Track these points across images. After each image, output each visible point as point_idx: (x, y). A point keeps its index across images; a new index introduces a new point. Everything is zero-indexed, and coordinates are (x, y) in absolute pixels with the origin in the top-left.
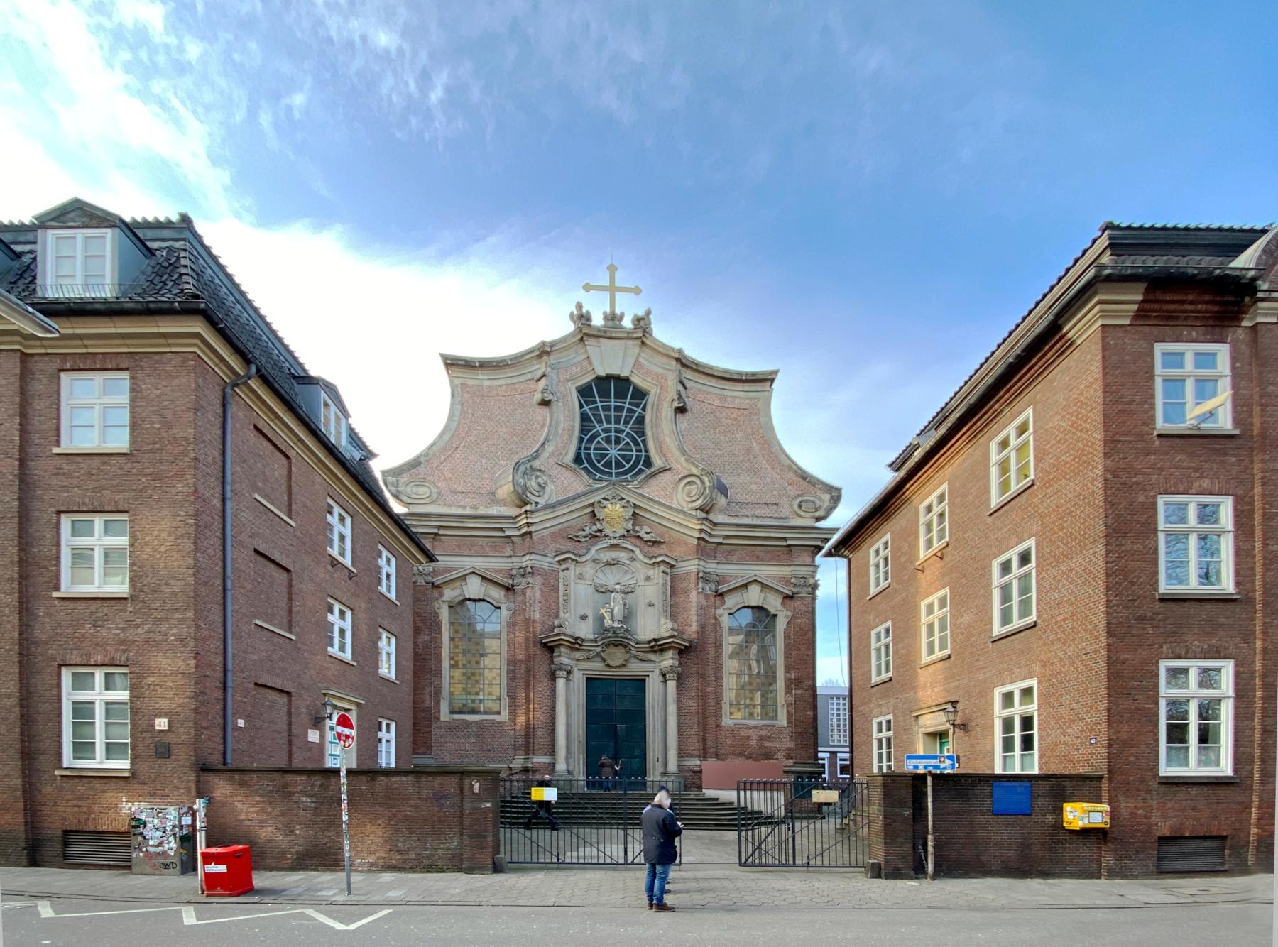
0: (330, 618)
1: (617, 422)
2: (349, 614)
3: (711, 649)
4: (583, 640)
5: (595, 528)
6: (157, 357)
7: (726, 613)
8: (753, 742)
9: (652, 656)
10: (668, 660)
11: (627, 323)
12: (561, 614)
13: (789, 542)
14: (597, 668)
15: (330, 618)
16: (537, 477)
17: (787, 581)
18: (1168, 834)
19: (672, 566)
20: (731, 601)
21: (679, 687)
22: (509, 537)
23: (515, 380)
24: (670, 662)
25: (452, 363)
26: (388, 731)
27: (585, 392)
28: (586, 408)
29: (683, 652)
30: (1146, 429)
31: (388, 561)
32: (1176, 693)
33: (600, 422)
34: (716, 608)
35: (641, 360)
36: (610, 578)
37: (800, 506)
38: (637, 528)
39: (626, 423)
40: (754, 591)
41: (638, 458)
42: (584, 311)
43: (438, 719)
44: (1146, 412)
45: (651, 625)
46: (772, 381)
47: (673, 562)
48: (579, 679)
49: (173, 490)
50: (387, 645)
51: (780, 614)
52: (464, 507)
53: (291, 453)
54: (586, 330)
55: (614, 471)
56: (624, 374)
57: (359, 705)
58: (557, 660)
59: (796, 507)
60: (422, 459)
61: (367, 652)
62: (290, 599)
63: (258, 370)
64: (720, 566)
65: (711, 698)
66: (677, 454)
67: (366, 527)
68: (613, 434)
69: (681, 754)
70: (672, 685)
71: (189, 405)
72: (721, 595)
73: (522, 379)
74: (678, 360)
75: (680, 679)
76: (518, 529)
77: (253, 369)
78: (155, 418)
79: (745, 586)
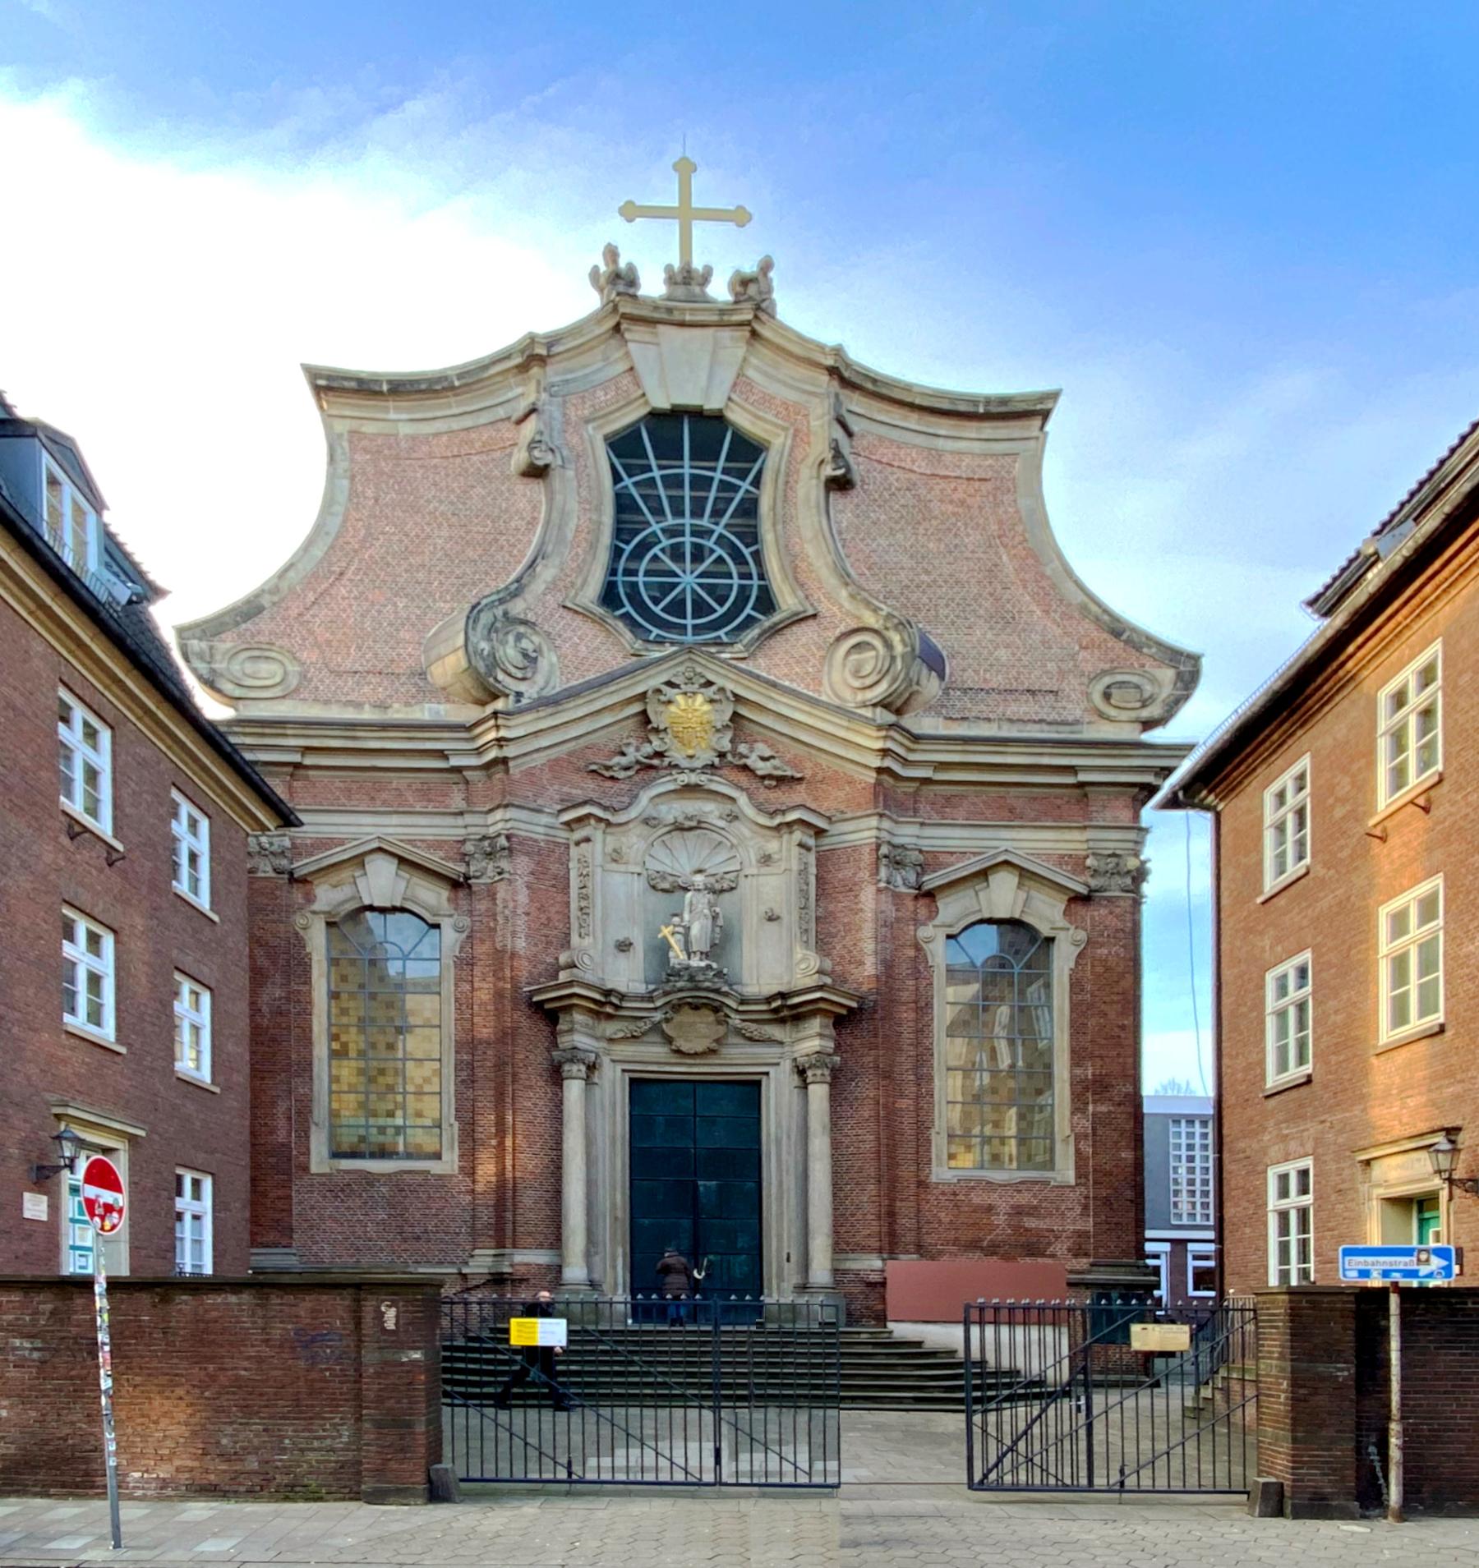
3: (906, 1015)
5: (648, 749)
8: (1000, 1220)
10: (812, 1040)
11: (719, 290)
12: (575, 939)
13: (1083, 777)
14: (653, 1057)
17: (1077, 864)
26: (197, 1195)
28: (628, 482)
29: (844, 1021)
31: (193, 824)
41: (744, 593)
42: (622, 264)
43: (306, 1169)
46: (1045, 415)
48: (613, 1082)
50: (193, 1011)
52: (358, 705)
56: (712, 404)
57: (132, 1139)
61: (147, 1022)
65: (907, 1124)
68: (688, 539)
69: (841, 1245)
70: (819, 1093)
72: (930, 895)
74: (833, 371)
79: (983, 874)
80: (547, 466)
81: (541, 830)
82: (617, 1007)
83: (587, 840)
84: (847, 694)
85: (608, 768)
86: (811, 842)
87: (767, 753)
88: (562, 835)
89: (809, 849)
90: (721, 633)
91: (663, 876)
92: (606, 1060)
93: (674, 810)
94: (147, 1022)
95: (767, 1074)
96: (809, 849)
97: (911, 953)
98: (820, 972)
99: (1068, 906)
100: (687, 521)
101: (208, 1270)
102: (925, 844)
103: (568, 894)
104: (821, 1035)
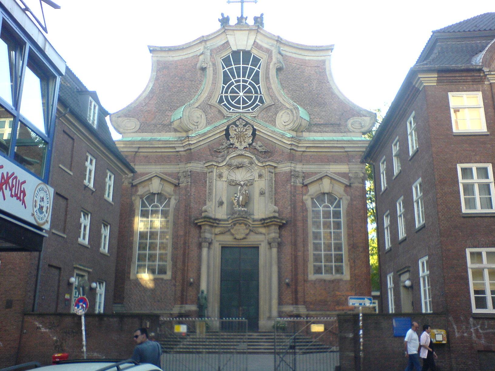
1: (244, 76)
3: (300, 224)
4: (220, 220)
5: (229, 142)
9: (263, 230)
10: (273, 233)
11: (251, 22)
12: (207, 202)
14: (227, 239)
17: (344, 175)
19: (275, 167)
21: (279, 252)
24: (273, 235)
27: (227, 61)
28: (226, 69)
29: (281, 227)
33: (234, 77)
34: (303, 195)
35: (257, 41)
36: (240, 176)
40: (326, 182)
41: (256, 98)
43: (129, 278)
45: (261, 209)
46: (332, 49)
48: (217, 247)
50: (106, 232)
51: (344, 198)
55: (241, 106)
56: (248, 49)
57: (89, 272)
61: (95, 236)
62: (66, 215)
63: (70, 110)
64: (305, 166)
65: (300, 261)
68: (241, 83)
69: (280, 303)
70: (275, 250)
74: (277, 41)
75: (280, 245)
77: (68, 109)
79: (321, 179)
80: (206, 68)
81: (199, 169)
82: (218, 224)
83: (212, 172)
86: (273, 171)
87: (261, 144)
88: (206, 170)
89: (272, 173)
90: (250, 109)
91: (233, 181)
92: (214, 241)
93: (235, 162)
94: (95, 236)
96: (272, 173)
97: (301, 204)
98: (275, 212)
99: (345, 189)
100: (241, 79)
101: (102, 311)
102: (304, 170)
103: (206, 188)
104: (275, 232)
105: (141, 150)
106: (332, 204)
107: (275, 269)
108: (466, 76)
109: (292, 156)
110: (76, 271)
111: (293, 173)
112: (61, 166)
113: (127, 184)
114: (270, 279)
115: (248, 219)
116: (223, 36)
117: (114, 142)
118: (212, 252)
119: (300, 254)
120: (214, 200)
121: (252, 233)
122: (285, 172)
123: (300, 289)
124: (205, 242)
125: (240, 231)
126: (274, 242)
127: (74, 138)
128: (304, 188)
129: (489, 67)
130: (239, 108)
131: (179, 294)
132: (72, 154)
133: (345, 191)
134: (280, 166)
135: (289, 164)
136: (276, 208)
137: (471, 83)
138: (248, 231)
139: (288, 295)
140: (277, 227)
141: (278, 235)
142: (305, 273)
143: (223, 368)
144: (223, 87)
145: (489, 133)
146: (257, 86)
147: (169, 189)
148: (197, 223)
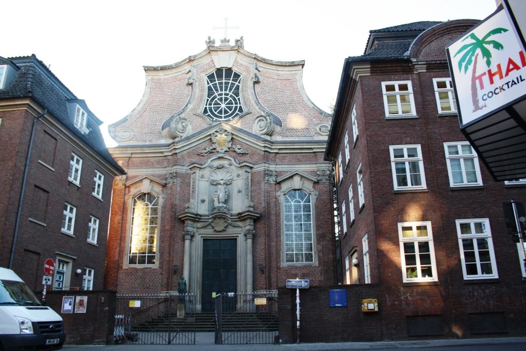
0: (65, 212)
1: (226, 90)
2: (75, 210)
3: (273, 217)
4: (201, 216)
5: (211, 148)
6: (12, 112)
7: (282, 194)
9: (240, 224)
10: (248, 226)
11: (232, 43)
12: (191, 200)
13: (315, 150)
14: (209, 232)
15: (65, 212)
16: (182, 123)
18: (411, 314)
19: (251, 168)
20: (285, 187)
22: (166, 156)
23: (176, 74)
24: (248, 227)
25: (147, 69)
26: (90, 274)
27: (211, 77)
28: (211, 84)
29: (256, 220)
30: (382, 117)
32: (466, 236)
33: (217, 90)
35: (238, 59)
36: (220, 176)
37: (320, 129)
38: (234, 147)
39: (231, 89)
40: (297, 179)
41: (236, 108)
44: (381, 110)
45: (239, 205)
46: (303, 65)
47: (251, 166)
48: (198, 240)
49: (7, 165)
53: (58, 138)
54: (211, 49)
57: (74, 259)
58: (186, 229)
59: (318, 129)
60: (128, 118)
61: (82, 228)
63: (48, 111)
64: (278, 166)
65: (274, 250)
66: (254, 105)
67: (90, 163)
70: (250, 241)
71: (20, 130)
73: (181, 73)
75: (254, 238)
76: (171, 151)
77: (46, 111)
78: (7, 136)
79: (291, 177)
80: (192, 83)
81: (184, 171)
83: (195, 173)
84: (258, 132)
85: (201, 153)
89: (249, 173)
91: (214, 181)
92: (196, 234)
93: (216, 163)
94: (82, 228)
95: (238, 236)
96: (249, 173)
102: (277, 170)
104: (249, 225)
105: (133, 156)
106: (302, 199)
107: (250, 257)
108: (397, 66)
109: (267, 156)
110: (58, 258)
111: (266, 172)
112: (40, 161)
113: (121, 186)
114: (246, 266)
115: (227, 214)
116: (208, 57)
117: (107, 150)
118: (194, 244)
119: (273, 244)
120: (196, 198)
121: (230, 227)
122: (260, 172)
123: (273, 276)
124: (188, 234)
125: (220, 225)
126: (249, 234)
127: (57, 138)
128: (277, 186)
129: (416, 58)
130: (221, 117)
131: (165, 281)
132: (55, 153)
133: (314, 187)
134: (255, 167)
135: (263, 165)
136: (252, 204)
137: (401, 73)
138: (226, 224)
139: (262, 280)
140: (252, 221)
141: (253, 227)
142: (278, 260)
143: (173, 340)
144: (208, 100)
145: (418, 117)
146: (237, 98)
147: (158, 189)
148: (181, 218)
